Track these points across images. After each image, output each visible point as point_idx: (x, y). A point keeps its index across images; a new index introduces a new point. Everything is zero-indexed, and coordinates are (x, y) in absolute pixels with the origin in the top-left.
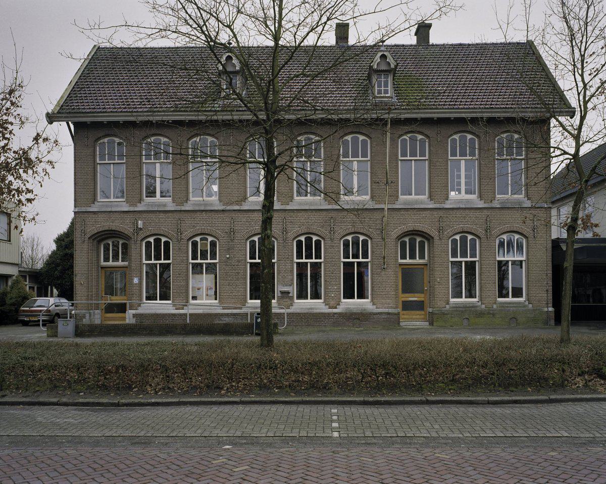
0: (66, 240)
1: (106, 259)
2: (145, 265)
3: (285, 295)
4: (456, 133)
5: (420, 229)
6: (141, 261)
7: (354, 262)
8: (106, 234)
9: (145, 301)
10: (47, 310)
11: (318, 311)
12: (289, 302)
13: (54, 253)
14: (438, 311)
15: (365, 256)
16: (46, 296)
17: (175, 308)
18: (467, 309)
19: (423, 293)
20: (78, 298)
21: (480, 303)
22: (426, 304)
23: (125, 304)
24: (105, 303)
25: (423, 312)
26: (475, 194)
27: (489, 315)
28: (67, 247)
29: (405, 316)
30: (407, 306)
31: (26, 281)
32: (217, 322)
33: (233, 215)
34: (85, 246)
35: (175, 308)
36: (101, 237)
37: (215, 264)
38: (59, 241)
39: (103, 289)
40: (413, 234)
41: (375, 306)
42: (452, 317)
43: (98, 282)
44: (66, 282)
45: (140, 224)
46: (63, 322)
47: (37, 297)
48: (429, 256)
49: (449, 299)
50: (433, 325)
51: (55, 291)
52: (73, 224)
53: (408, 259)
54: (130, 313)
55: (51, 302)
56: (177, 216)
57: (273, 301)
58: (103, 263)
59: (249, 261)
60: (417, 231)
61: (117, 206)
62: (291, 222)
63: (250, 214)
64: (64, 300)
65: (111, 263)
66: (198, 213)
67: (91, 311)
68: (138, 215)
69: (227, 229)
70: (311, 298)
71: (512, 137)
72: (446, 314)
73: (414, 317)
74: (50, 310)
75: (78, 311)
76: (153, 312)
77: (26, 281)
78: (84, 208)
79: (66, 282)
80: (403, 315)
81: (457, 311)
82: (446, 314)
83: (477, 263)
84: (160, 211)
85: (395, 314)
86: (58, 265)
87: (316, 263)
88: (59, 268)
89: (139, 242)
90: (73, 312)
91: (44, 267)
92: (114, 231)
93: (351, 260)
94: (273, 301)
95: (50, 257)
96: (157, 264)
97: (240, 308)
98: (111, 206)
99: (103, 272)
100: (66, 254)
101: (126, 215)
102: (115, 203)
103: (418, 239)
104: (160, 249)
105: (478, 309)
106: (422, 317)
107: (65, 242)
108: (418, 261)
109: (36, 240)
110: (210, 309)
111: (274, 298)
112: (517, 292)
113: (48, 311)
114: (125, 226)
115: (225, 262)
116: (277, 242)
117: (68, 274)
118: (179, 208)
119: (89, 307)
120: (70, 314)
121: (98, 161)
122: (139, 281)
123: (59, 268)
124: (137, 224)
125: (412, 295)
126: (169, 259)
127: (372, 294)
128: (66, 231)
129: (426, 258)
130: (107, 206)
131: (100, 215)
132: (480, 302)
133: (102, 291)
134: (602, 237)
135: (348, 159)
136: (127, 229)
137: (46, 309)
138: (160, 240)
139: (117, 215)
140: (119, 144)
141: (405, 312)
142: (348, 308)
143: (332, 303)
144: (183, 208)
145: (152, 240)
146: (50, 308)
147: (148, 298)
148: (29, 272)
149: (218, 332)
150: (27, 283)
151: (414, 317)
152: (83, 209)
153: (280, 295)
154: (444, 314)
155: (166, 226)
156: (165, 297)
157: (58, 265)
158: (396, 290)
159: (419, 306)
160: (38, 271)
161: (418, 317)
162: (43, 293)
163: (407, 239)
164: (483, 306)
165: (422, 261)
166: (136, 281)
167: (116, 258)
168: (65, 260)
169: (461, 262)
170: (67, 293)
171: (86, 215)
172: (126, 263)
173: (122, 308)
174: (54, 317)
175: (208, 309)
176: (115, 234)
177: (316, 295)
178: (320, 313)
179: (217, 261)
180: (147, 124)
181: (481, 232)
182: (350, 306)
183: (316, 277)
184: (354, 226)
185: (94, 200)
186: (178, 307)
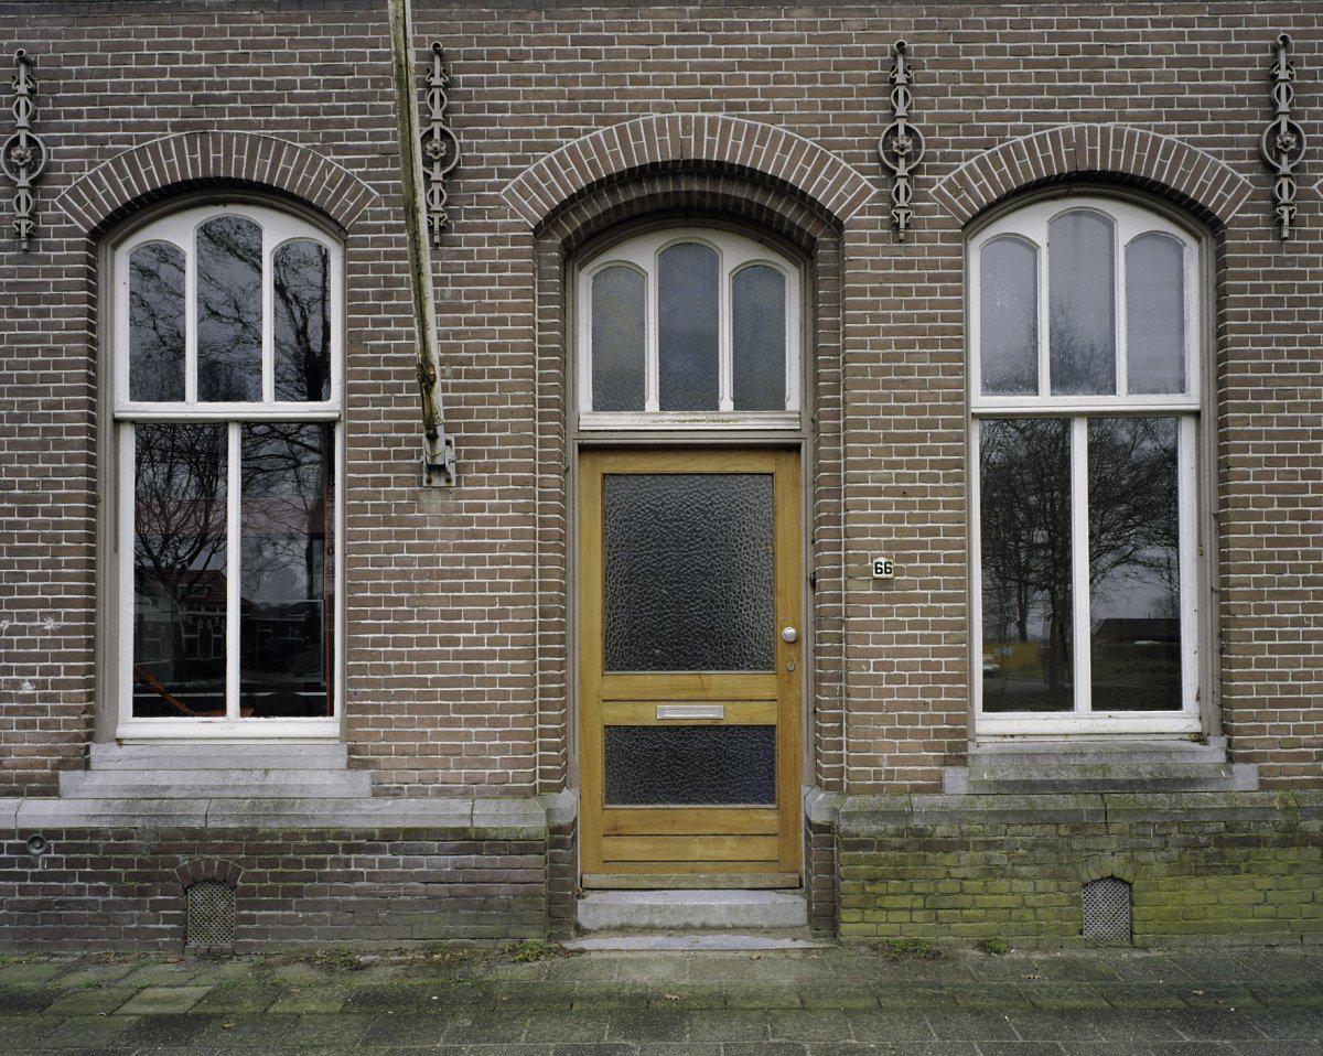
2: (128, 442)
5: (734, 151)
7: (220, 427)
14: (873, 815)
15: (309, 376)
18: (1115, 800)
19: (767, 664)
21: (1214, 752)
22: (796, 749)
25: (763, 816)
27: (1291, 855)
29: (629, 848)
30: (658, 767)
41: (364, 778)
42: (990, 871)
48: (812, 381)
49: (968, 720)
50: (834, 932)
53: (652, 403)
58: (593, 420)
59: (982, 402)
72: (948, 846)
73: (698, 850)
80: (615, 832)
81: (1029, 817)
82: (948, 846)
83: (1187, 432)
85: (525, 846)
89: (63, 253)
93: (192, 407)
105: (1204, 795)
106: (763, 849)
108: (726, 418)
112: (1140, 664)
116: (346, 256)
125: (683, 678)
129: (793, 401)
132: (1217, 745)
141: (628, 813)
142: (149, 793)
151: (698, 850)
154: (924, 842)
158: (552, 639)
159: (725, 766)
161: (728, 849)
164: (1245, 777)
165: (758, 424)
179: (329, 407)
182: (162, 779)
184: (198, 132)
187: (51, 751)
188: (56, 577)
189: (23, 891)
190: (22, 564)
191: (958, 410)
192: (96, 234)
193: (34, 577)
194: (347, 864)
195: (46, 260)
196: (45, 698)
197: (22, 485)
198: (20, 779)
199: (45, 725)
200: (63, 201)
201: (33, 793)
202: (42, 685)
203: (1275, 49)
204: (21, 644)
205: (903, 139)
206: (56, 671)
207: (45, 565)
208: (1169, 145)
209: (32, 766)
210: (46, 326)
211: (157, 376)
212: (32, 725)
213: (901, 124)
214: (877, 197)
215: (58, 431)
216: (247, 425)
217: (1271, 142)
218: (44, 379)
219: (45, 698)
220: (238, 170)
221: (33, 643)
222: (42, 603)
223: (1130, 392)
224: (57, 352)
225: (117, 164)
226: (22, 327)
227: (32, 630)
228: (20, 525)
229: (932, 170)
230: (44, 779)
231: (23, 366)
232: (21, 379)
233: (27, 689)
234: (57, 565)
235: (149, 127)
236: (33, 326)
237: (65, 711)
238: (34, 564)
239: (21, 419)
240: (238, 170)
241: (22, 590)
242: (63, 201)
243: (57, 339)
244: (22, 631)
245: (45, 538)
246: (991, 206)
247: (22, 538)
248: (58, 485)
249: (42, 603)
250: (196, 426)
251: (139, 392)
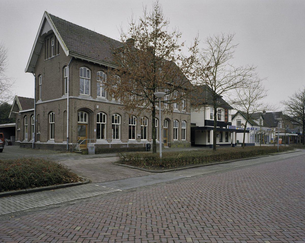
4: (83, 66)
7: (100, 124)
17: (108, 142)
21: (178, 141)
22: (167, 140)
26: (105, 97)
32: (121, 147)
35: (108, 142)
37: (134, 126)
40: (82, 111)
45: (98, 107)
57: (156, 140)
60: (90, 110)
70: (132, 139)
71: (117, 77)
75: (73, 143)
76: (101, 143)
78: (76, 97)
83: (105, 124)
84: (104, 102)
87: (103, 124)
94: (156, 140)
98: (86, 98)
101: (91, 102)
103: (84, 113)
104: (101, 118)
111: (156, 139)
126: (105, 122)
127: (121, 137)
134: (197, 125)
135: (99, 81)
136: (92, 108)
138: (102, 114)
139: (89, 102)
140: (88, 71)
163: (80, 113)
169: (131, 126)
171: (77, 100)
180: (97, 65)
181: (107, 112)
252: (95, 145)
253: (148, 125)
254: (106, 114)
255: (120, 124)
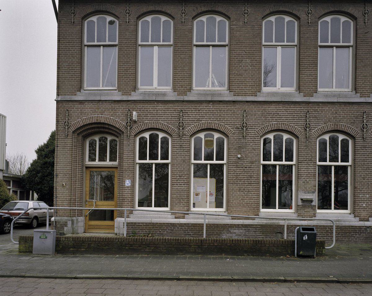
0: (46, 150)
1: (92, 159)
3: (307, 204)
6: (134, 160)
7: (331, 166)
8: (94, 128)
9: (137, 208)
10: (25, 213)
11: (347, 224)
12: (312, 213)
13: (35, 162)
15: (165, 157)
16: (28, 199)
17: (174, 216)
20: (59, 203)
23: (112, 211)
24: (90, 210)
28: (46, 156)
31: (10, 186)
32: (225, 236)
33: (246, 107)
34: (69, 141)
35: (174, 216)
36: (88, 131)
37: (345, 167)
38: (40, 151)
39: (88, 193)
43: (82, 184)
44: (45, 187)
46: (39, 234)
47: (20, 200)
51: (36, 196)
52: (53, 136)
54: (119, 221)
55: (32, 205)
56: (178, 107)
58: (88, 163)
60: (112, 126)
61: (108, 95)
62: (315, 117)
63: (266, 107)
64: (43, 205)
65: (97, 163)
66: (205, 105)
67: (74, 218)
68: (132, 106)
69: (238, 124)
70: (335, 209)
74: (28, 213)
76: (147, 220)
77: (10, 186)
79: (45, 187)
86: (38, 172)
88: (39, 175)
90: (53, 219)
91: (26, 174)
92: (103, 123)
95: (32, 165)
96: (152, 164)
97: (254, 219)
98: (101, 95)
99: (88, 172)
100: (46, 163)
101: (117, 106)
102: (105, 91)
107: (46, 153)
108: (108, 163)
109: (24, 158)
110: (216, 219)
113: (26, 214)
114: (116, 119)
115: (236, 163)
117: (47, 180)
118: (181, 98)
119: (72, 214)
120: (50, 220)
121: (86, 43)
122: (131, 184)
123: (39, 175)
124: (131, 115)
126: (292, 160)
127: (354, 203)
128: (46, 142)
130: (95, 95)
131: (87, 105)
133: (86, 194)
136: (119, 121)
137: (23, 212)
139: (107, 106)
140: (111, 23)
143: (364, 214)
144: (186, 98)
145: (147, 135)
146: (29, 211)
147: (141, 204)
148: (13, 177)
149: (246, 252)
150: (11, 187)
152: (68, 98)
153: (300, 203)
155: (165, 118)
156: (161, 202)
157: (38, 172)
160: (21, 177)
162: (25, 196)
166: (128, 183)
167: (102, 158)
168: (45, 167)
170: (48, 197)
172: (115, 163)
173: (109, 216)
174: (32, 221)
175: (213, 219)
176: (104, 128)
177: (341, 204)
178: (349, 226)
179: (224, 162)
183: (341, 184)
185: (80, 88)
186: (177, 215)
187: (368, 215)
188: (368, 189)
189: (366, 235)
190: (363, 187)
191: (315, 165)
192: (135, 135)
193: (365, 189)
194: (173, 228)
195: (367, 142)
196: (367, 207)
197: (363, 175)
198: (363, 219)
199: (367, 211)
200: (370, 133)
201: (365, 221)
202: (366, 205)
203: (364, 113)
204: (363, 199)
205: (308, 125)
206: (368, 203)
207: (367, 187)
208: (291, 125)
209: (365, 217)
210: (367, 152)
211: (197, 157)
212: (365, 211)
213: (308, 123)
214: (177, 132)
215: (369, 167)
216: (211, 165)
217: (306, 126)
218: (367, 159)
219: (367, 207)
220: (203, 127)
221: (365, 199)
222: (367, 193)
223: (274, 161)
224: (369, 155)
225: (139, 125)
226: (363, 152)
227: (365, 197)
228: (363, 181)
229: (312, 129)
230: (366, 219)
231: (364, 157)
232: (363, 159)
233: (364, 205)
234: (369, 187)
235: (270, 121)
236: (365, 152)
237: (370, 209)
238: (365, 187)
239: (363, 165)
240: (203, 127)
241: (363, 191)
242: (370, 133)
243: (369, 154)
244: (363, 197)
245: (367, 183)
246: (137, 133)
247: (363, 183)
248: (369, 175)
249: (367, 193)
250: (203, 164)
251: (140, 159)
252: (128, 224)
253: (354, 160)
254: (353, 137)
255: (350, 163)
